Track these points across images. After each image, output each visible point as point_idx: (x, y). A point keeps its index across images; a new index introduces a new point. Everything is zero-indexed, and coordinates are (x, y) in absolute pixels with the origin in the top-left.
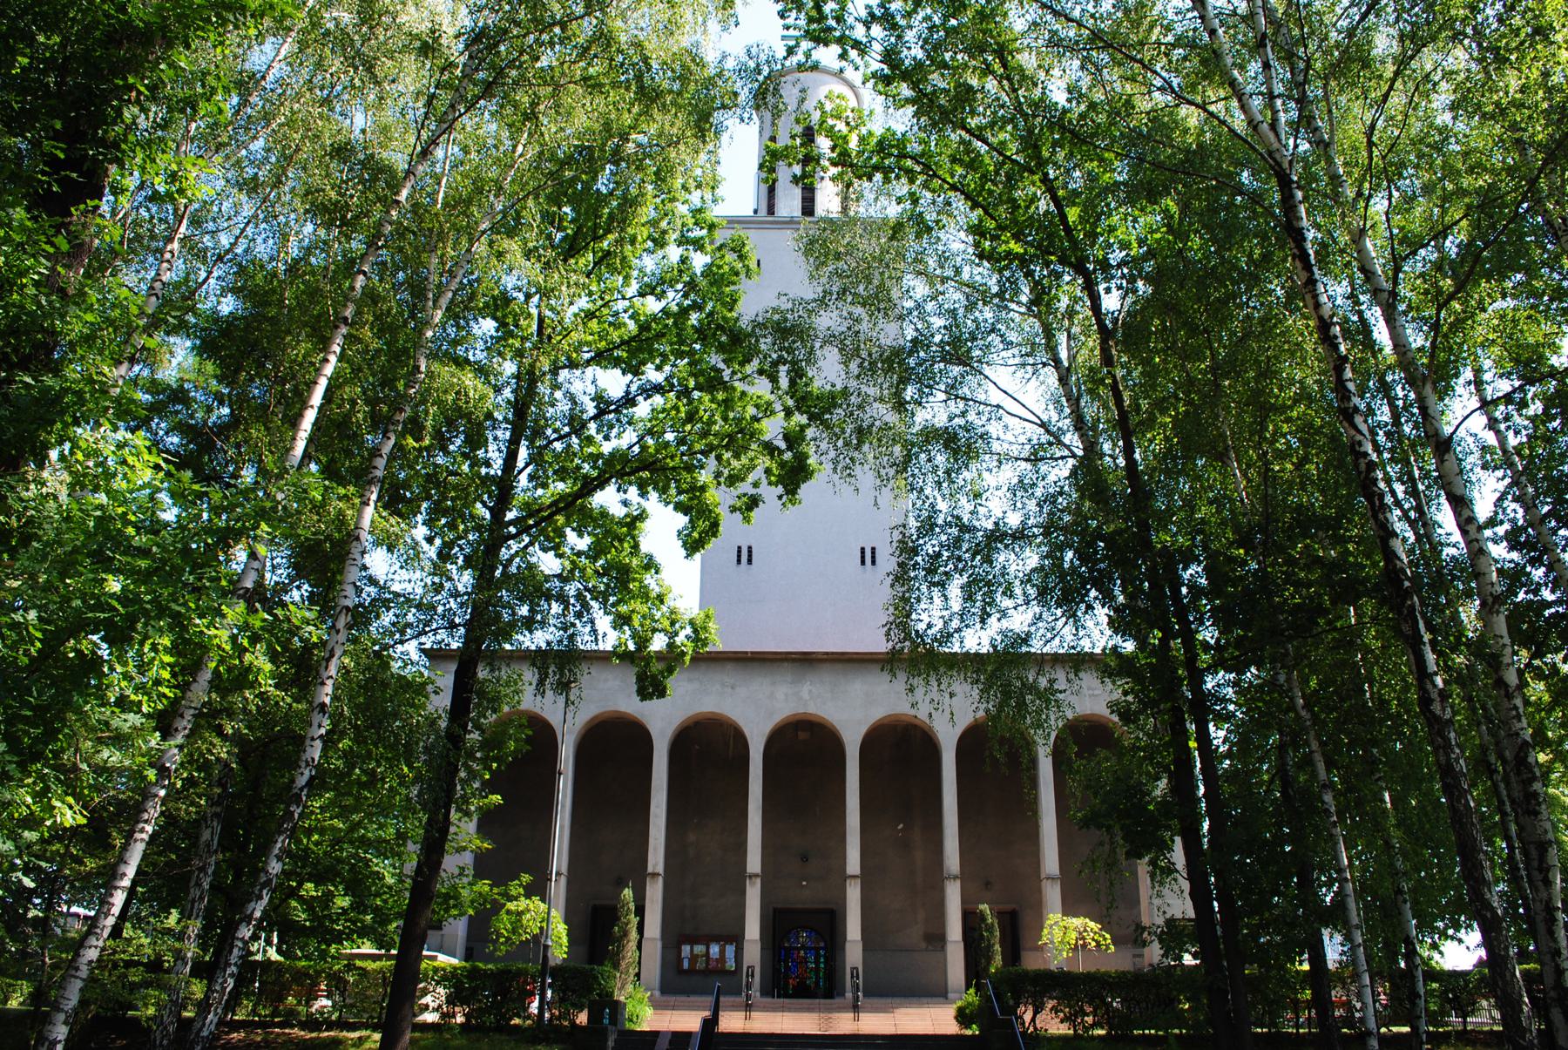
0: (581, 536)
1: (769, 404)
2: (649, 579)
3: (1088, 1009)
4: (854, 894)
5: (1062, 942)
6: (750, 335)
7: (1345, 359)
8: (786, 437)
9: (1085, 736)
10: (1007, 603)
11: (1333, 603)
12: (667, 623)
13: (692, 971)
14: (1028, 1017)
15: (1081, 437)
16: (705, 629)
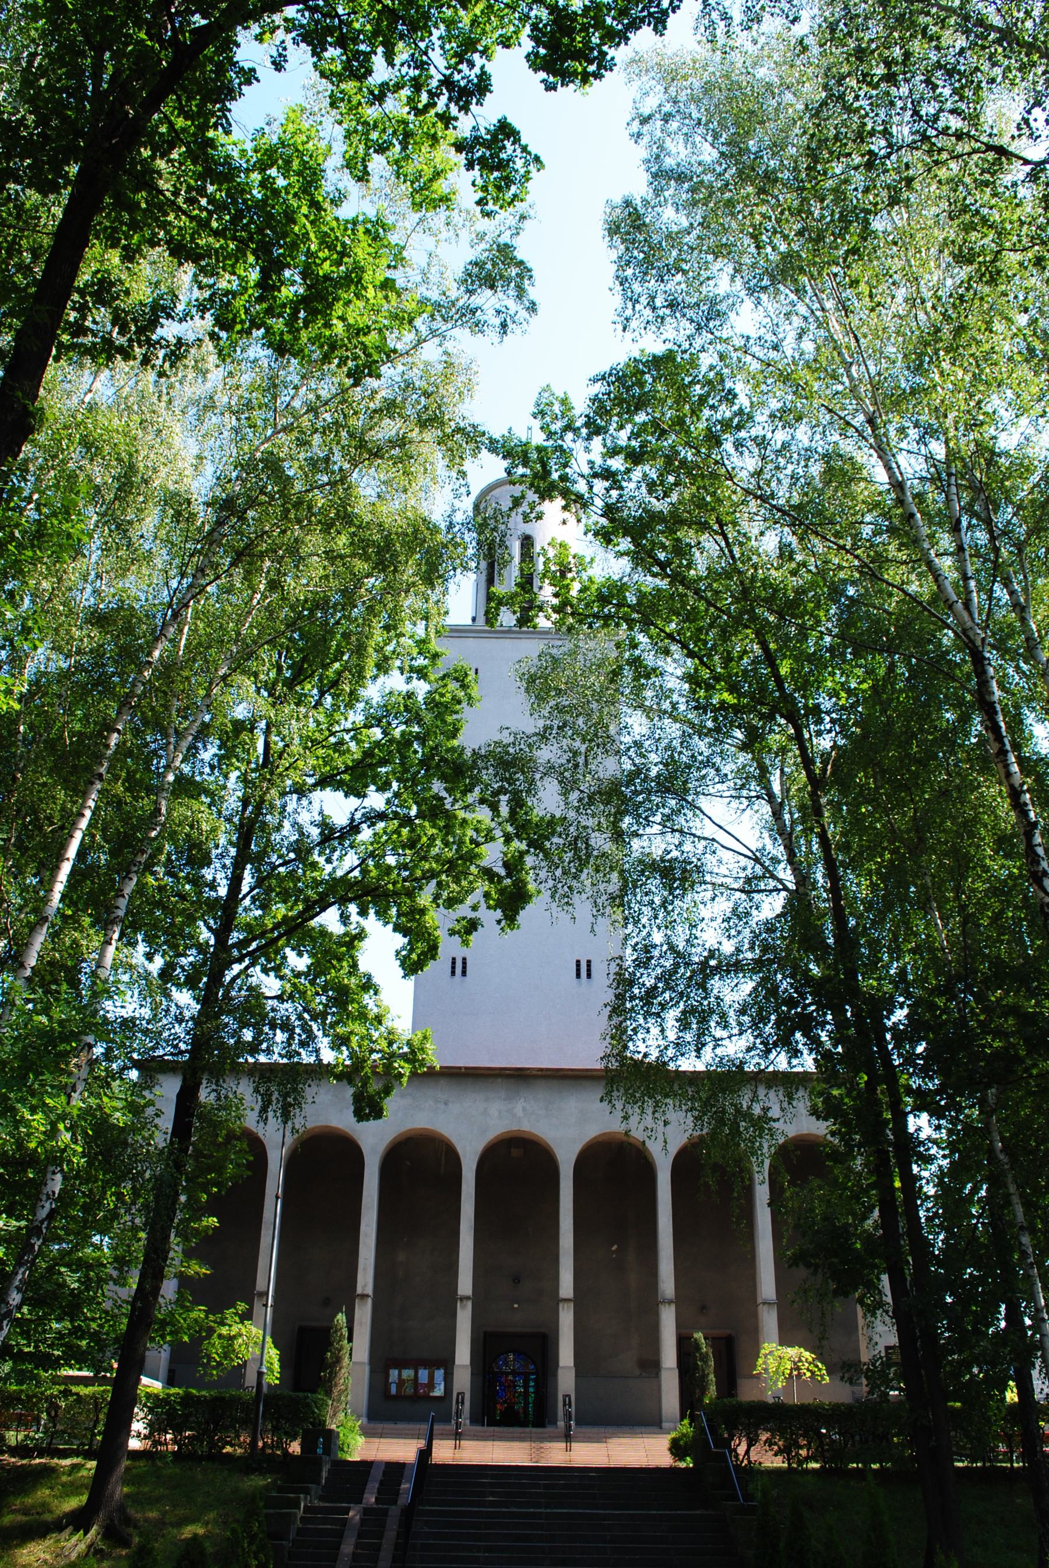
0: (300, 954)
1: (490, 830)
2: (367, 999)
3: (803, 1442)
4: (566, 1319)
5: (777, 1372)
6: (473, 768)
7: (1035, 825)
8: (506, 865)
9: (799, 1159)
10: (719, 1033)
11: (1029, 1053)
12: (384, 1044)
13: (398, 1397)
14: (741, 1450)
15: (794, 870)
16: (422, 1050)
